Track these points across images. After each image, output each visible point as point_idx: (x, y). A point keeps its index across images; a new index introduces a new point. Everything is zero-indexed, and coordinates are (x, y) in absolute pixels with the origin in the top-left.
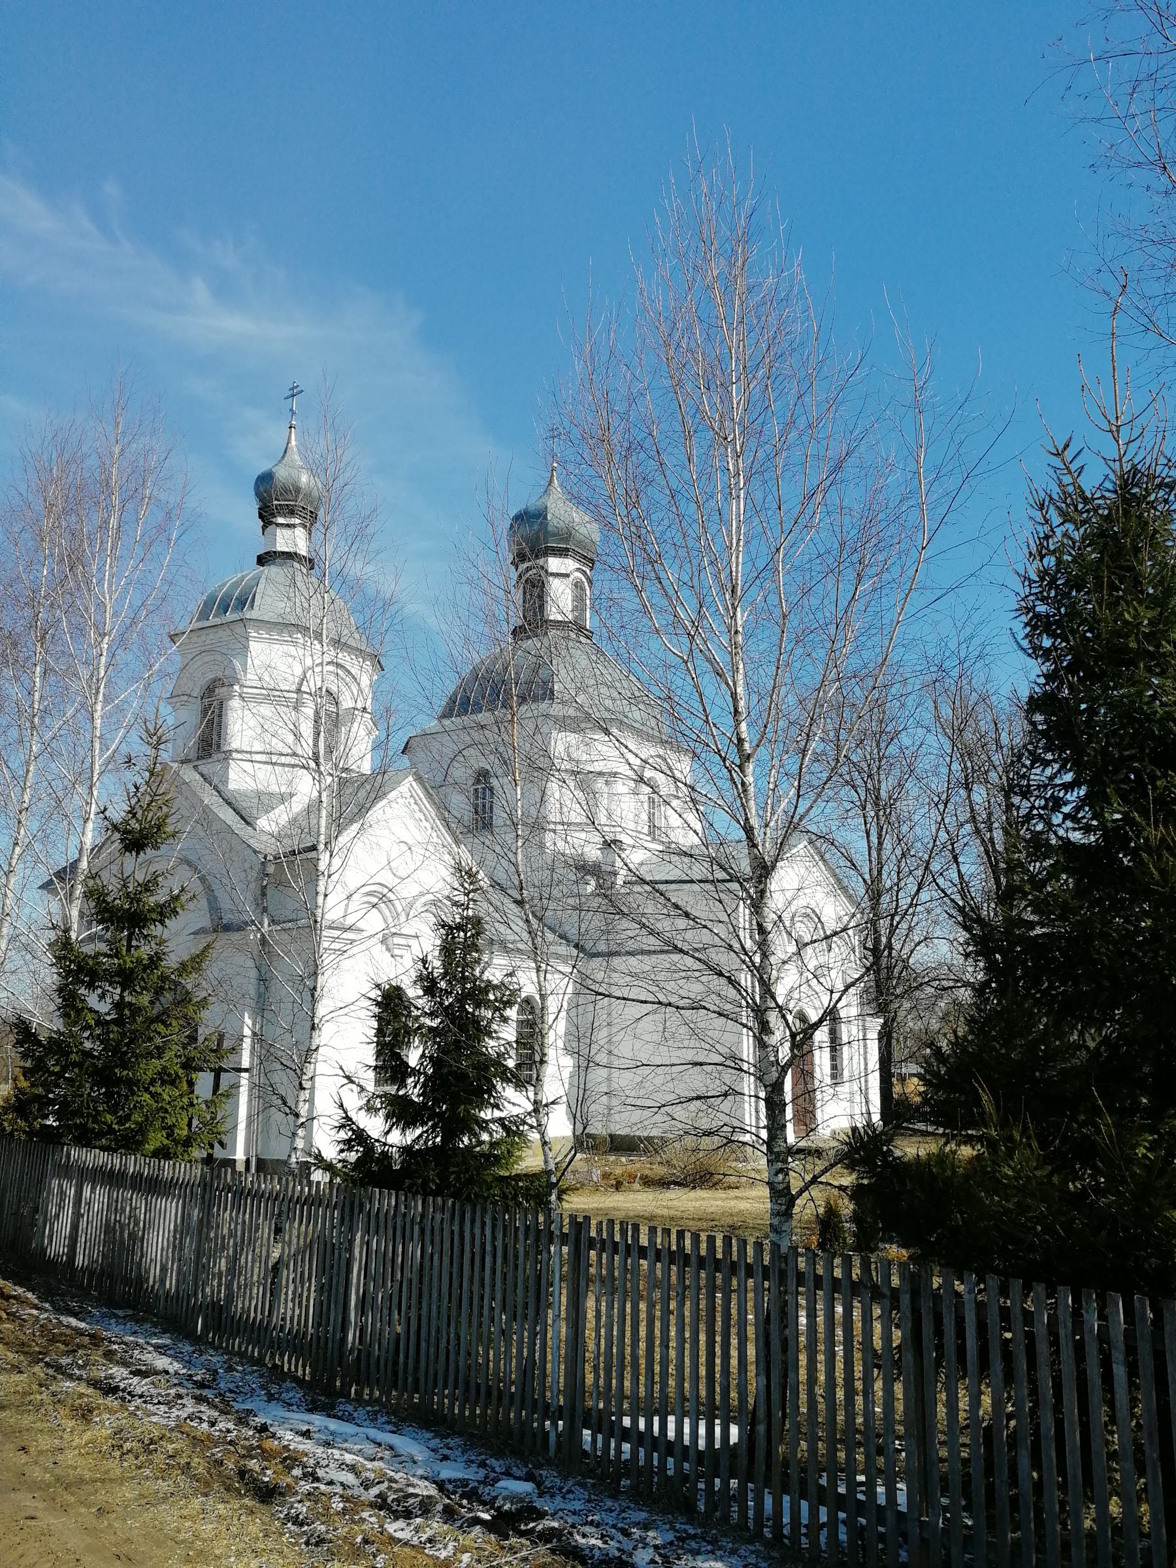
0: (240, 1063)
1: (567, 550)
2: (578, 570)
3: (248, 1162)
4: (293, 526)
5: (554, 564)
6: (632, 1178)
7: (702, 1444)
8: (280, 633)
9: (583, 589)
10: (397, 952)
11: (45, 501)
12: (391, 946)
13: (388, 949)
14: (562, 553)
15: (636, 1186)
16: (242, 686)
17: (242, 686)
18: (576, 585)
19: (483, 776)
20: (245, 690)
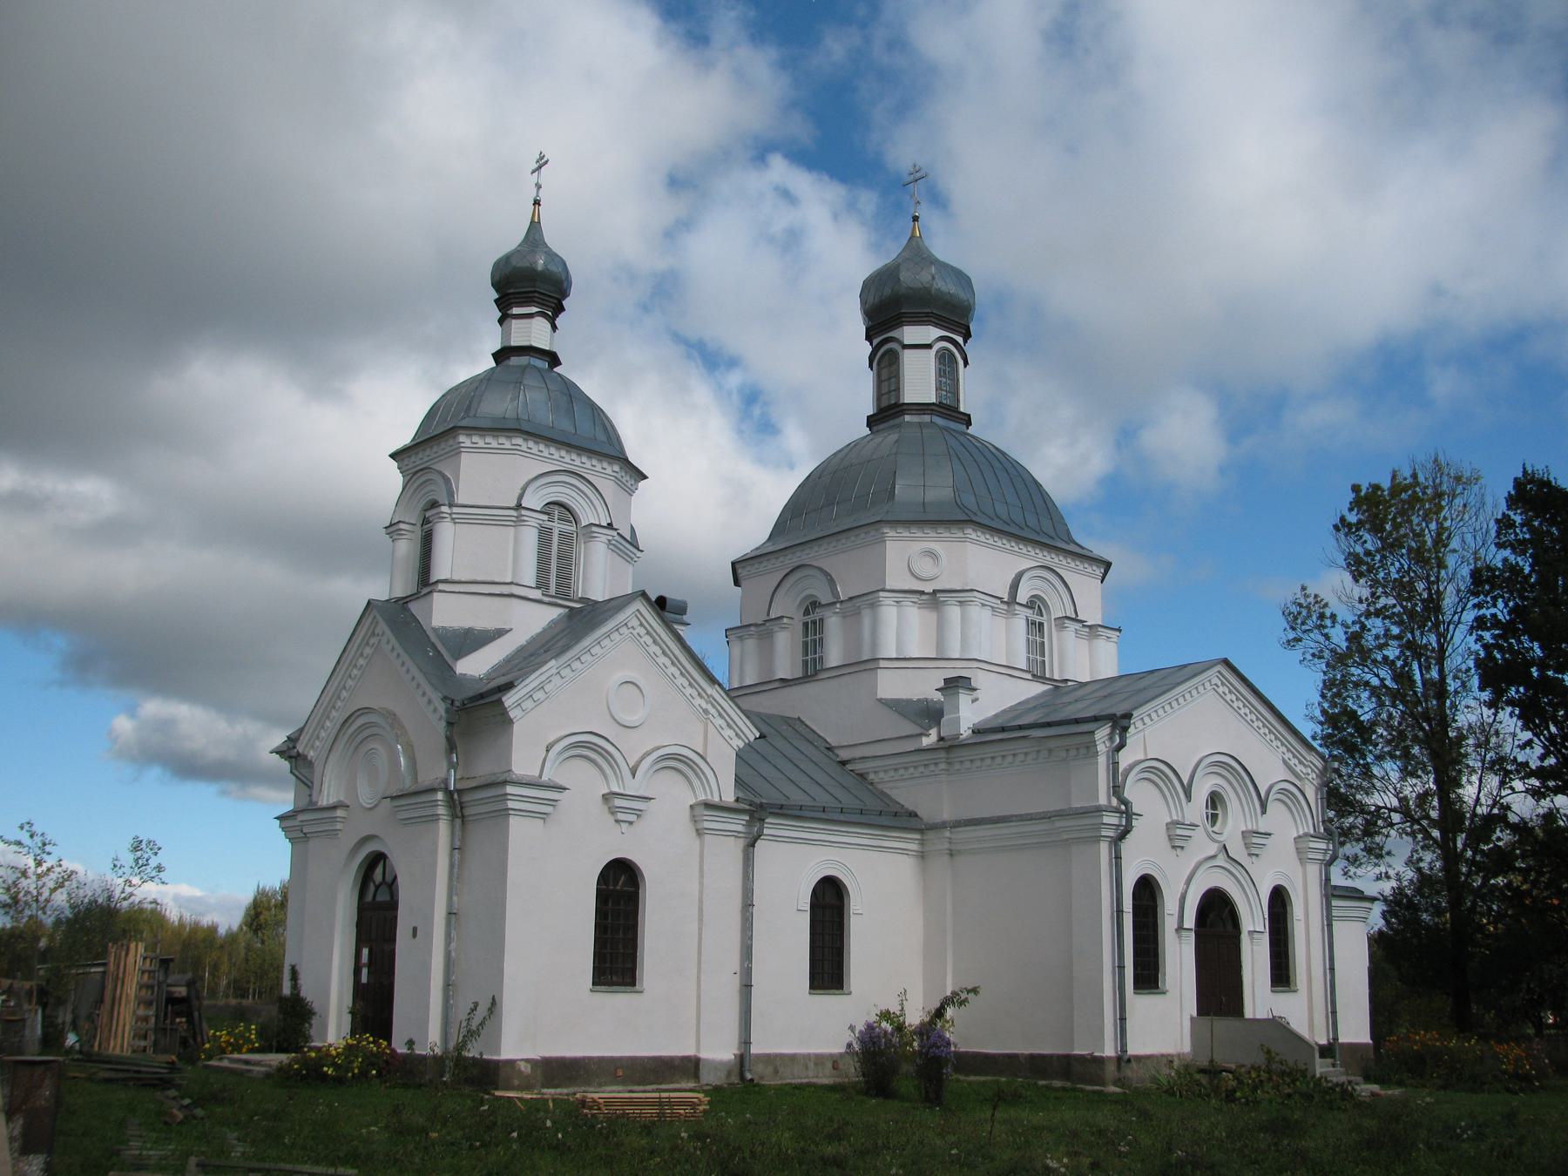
10: (621, 816)
13: (613, 813)
20: (455, 510)
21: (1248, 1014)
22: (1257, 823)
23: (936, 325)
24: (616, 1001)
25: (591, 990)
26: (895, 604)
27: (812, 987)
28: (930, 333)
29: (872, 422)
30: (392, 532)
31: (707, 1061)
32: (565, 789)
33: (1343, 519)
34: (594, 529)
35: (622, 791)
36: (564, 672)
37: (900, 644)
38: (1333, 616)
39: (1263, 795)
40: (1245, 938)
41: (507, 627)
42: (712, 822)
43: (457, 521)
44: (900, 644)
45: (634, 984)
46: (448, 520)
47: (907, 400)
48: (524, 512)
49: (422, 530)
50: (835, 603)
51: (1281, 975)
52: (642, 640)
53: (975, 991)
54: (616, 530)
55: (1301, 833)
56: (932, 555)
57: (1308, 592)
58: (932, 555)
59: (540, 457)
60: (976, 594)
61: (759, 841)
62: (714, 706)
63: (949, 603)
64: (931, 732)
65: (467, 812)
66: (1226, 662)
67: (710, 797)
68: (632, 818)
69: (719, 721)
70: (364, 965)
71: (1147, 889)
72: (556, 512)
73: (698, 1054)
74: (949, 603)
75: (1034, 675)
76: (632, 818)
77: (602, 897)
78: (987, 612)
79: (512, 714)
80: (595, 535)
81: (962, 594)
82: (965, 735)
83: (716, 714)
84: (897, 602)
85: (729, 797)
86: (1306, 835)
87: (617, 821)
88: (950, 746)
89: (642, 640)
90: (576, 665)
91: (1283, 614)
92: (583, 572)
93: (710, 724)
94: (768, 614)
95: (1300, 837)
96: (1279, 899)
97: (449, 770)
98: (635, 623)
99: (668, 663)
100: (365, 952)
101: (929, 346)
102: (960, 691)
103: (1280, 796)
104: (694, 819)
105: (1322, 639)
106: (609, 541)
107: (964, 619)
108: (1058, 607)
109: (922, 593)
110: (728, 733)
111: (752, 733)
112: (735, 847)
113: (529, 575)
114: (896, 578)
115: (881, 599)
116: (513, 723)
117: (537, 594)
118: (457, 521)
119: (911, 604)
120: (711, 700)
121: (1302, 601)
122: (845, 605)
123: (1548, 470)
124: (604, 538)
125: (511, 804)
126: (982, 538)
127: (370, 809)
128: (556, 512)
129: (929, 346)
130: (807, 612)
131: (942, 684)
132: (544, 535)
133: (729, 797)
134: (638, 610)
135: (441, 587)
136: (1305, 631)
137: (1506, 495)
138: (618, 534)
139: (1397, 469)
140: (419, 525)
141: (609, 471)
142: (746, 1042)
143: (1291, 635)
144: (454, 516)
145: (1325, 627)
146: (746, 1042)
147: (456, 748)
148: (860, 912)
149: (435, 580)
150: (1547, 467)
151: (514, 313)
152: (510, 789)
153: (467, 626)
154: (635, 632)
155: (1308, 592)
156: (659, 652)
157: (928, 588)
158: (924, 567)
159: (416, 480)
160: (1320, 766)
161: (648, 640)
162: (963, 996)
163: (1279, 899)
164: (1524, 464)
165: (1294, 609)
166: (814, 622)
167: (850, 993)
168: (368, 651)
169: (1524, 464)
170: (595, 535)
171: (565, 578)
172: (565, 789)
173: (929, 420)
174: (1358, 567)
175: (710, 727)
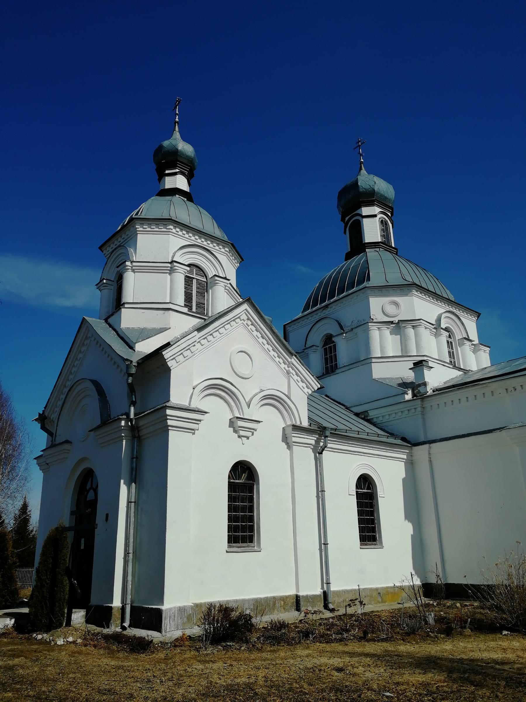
0: (320, 596)
1: (374, 201)
2: (381, 213)
3: (123, 609)
4: (175, 174)
5: (366, 211)
6: (462, 622)
7: (473, 349)
8: (157, 225)
9: (386, 223)
10: (242, 433)
11: (517, 650)
12: (237, 429)
13: (235, 431)
14: (370, 204)
15: (468, 631)
16: (132, 262)
17: (132, 262)
18: (382, 222)
19: (329, 340)
20: (134, 264)
23: (378, 206)
25: (227, 552)
26: (377, 329)
28: (376, 210)
30: (100, 286)
31: (303, 596)
32: (206, 413)
34: (217, 278)
35: (242, 417)
36: (203, 342)
41: (168, 327)
42: (297, 437)
43: (135, 270)
46: (130, 270)
47: (366, 242)
48: (175, 264)
49: (117, 285)
50: (343, 333)
52: (249, 328)
54: (229, 280)
56: (396, 304)
58: (396, 304)
59: (182, 237)
60: (422, 321)
61: (324, 451)
63: (407, 327)
64: (408, 392)
65: (142, 433)
67: (294, 423)
68: (249, 434)
69: (296, 377)
72: (195, 270)
73: (298, 593)
74: (407, 327)
76: (249, 434)
77: (232, 487)
78: (428, 331)
79: (170, 364)
80: (217, 282)
81: (414, 323)
82: (429, 393)
83: (294, 373)
84: (378, 328)
85: (305, 423)
87: (239, 437)
89: (249, 328)
90: (210, 338)
92: (212, 298)
93: (291, 379)
94: (305, 346)
97: (130, 406)
98: (244, 317)
99: (265, 342)
102: (424, 368)
104: (285, 439)
106: (225, 286)
107: (416, 335)
108: (458, 336)
109: (392, 322)
110: (301, 384)
112: (310, 454)
113: (181, 299)
115: (370, 327)
116: (171, 370)
117: (185, 310)
118: (135, 270)
119: (387, 329)
120: (290, 365)
122: (347, 334)
124: (222, 284)
125: (138, 232)
126: (420, 295)
127: (83, 441)
128: (195, 270)
131: (412, 366)
132: (188, 280)
133: (305, 423)
134: (246, 310)
135: (126, 306)
138: (230, 284)
140: (116, 282)
141: (223, 250)
142: (326, 582)
144: (134, 268)
146: (326, 582)
147: (135, 392)
148: (383, 496)
149: (123, 302)
151: (167, 187)
152: (169, 412)
153: (142, 326)
154: (245, 323)
156: (260, 336)
157: (396, 320)
158: (391, 309)
159: (113, 256)
161: (254, 329)
168: (84, 348)
170: (217, 282)
171: (201, 306)
172: (206, 413)
175: (292, 381)
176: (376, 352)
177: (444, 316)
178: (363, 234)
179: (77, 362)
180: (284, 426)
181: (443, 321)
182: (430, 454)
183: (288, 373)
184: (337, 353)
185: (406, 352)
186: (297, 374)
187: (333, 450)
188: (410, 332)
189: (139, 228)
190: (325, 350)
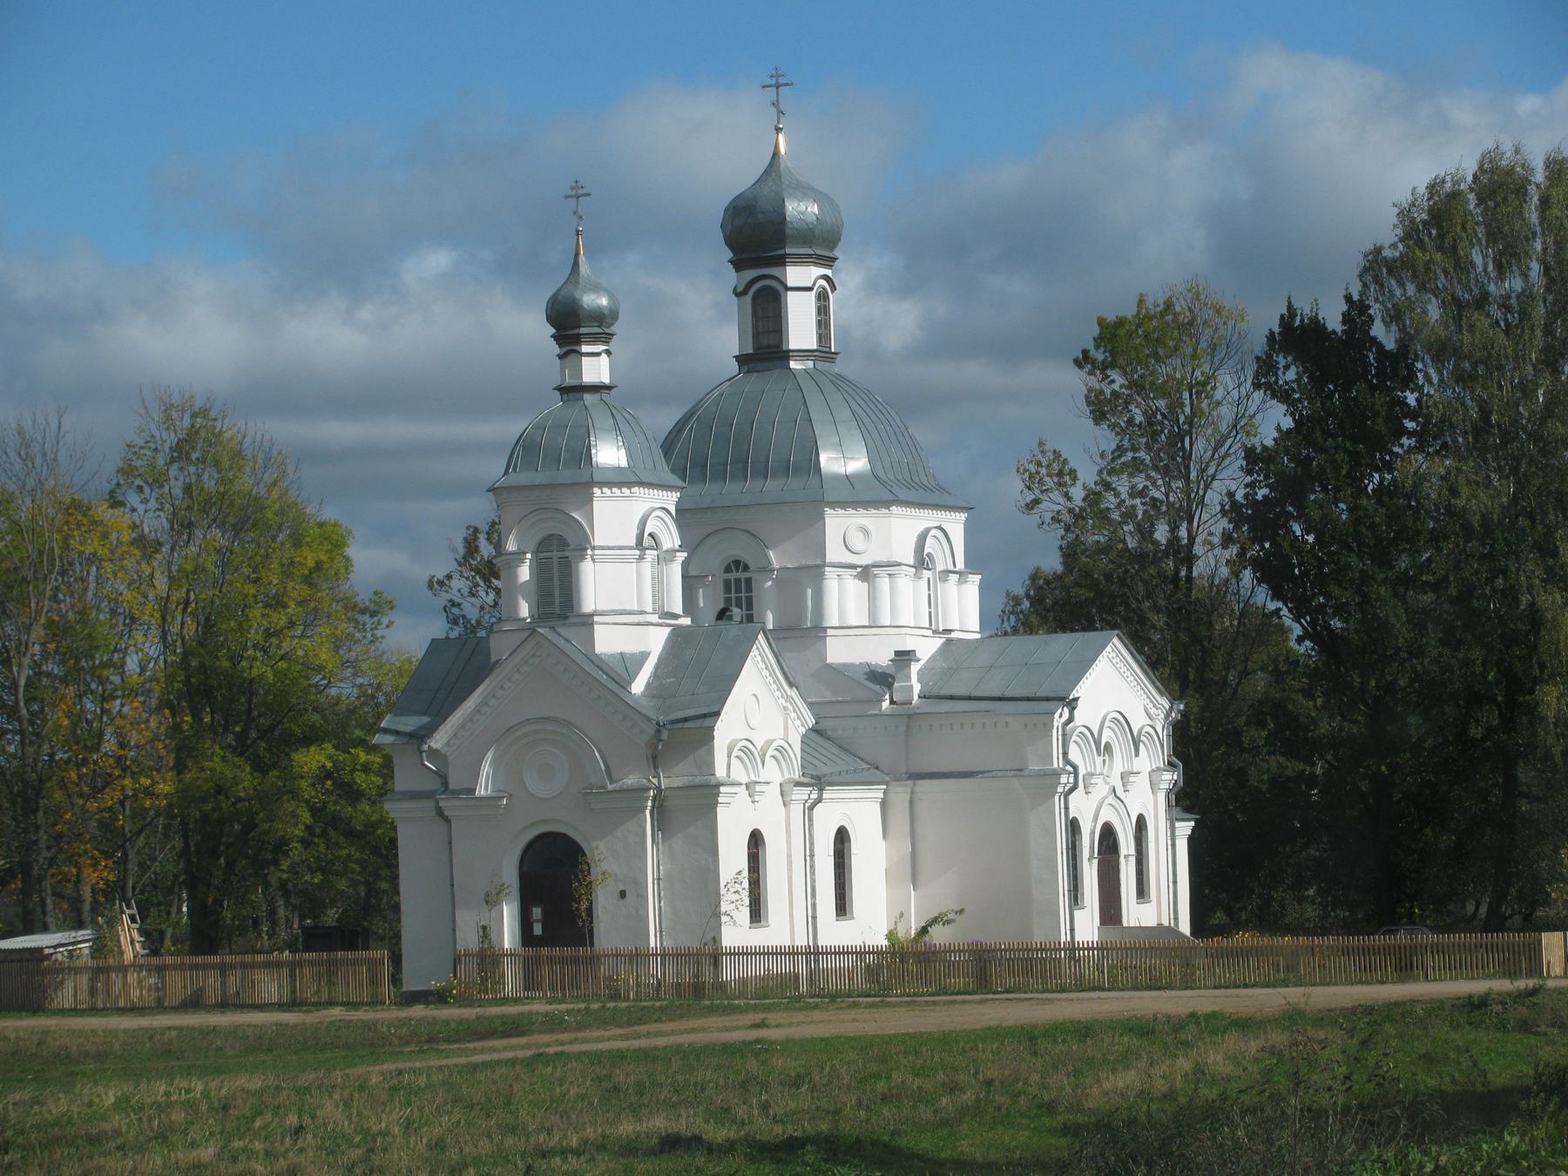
20: (597, 552)
21: (1125, 924)
22: (1132, 763)
23: (816, 264)
24: (844, 924)
27: (837, 915)
29: (741, 359)
33: (1085, 353)
35: (758, 780)
37: (842, 614)
38: (1073, 473)
39: (1135, 733)
40: (1122, 859)
44: (842, 614)
45: (845, 915)
47: (791, 347)
51: (1142, 892)
53: (961, 912)
55: (1154, 767)
56: (865, 531)
57: (1046, 448)
62: (791, 704)
66: (940, 528)
69: (793, 715)
70: (538, 921)
71: (1074, 827)
75: (934, 632)
86: (1158, 769)
88: (907, 717)
91: (1018, 471)
95: (1153, 771)
96: (1141, 824)
100: (537, 912)
101: (809, 289)
103: (1113, 725)
105: (1062, 500)
109: (854, 567)
111: (811, 721)
114: (834, 552)
120: (788, 698)
121: (1040, 457)
123: (1317, 304)
129: (809, 289)
130: (728, 570)
136: (1042, 492)
137: (1267, 333)
139: (1144, 293)
143: (1030, 497)
145: (1065, 485)
150: (1316, 300)
155: (1046, 448)
160: (1167, 707)
162: (951, 916)
163: (1141, 824)
164: (1289, 298)
165: (1033, 468)
166: (738, 581)
167: (853, 918)
169: (1289, 298)
173: (812, 366)
174: (1100, 409)
176: (832, 618)
177: (933, 532)
178: (783, 318)
179: (517, 676)
180: (781, 780)
181: (929, 541)
182: (912, 793)
183: (785, 708)
184: (754, 593)
185: (874, 621)
186: (794, 711)
187: (1128, 922)
188: (884, 583)
189: (597, 491)
190: (727, 584)
